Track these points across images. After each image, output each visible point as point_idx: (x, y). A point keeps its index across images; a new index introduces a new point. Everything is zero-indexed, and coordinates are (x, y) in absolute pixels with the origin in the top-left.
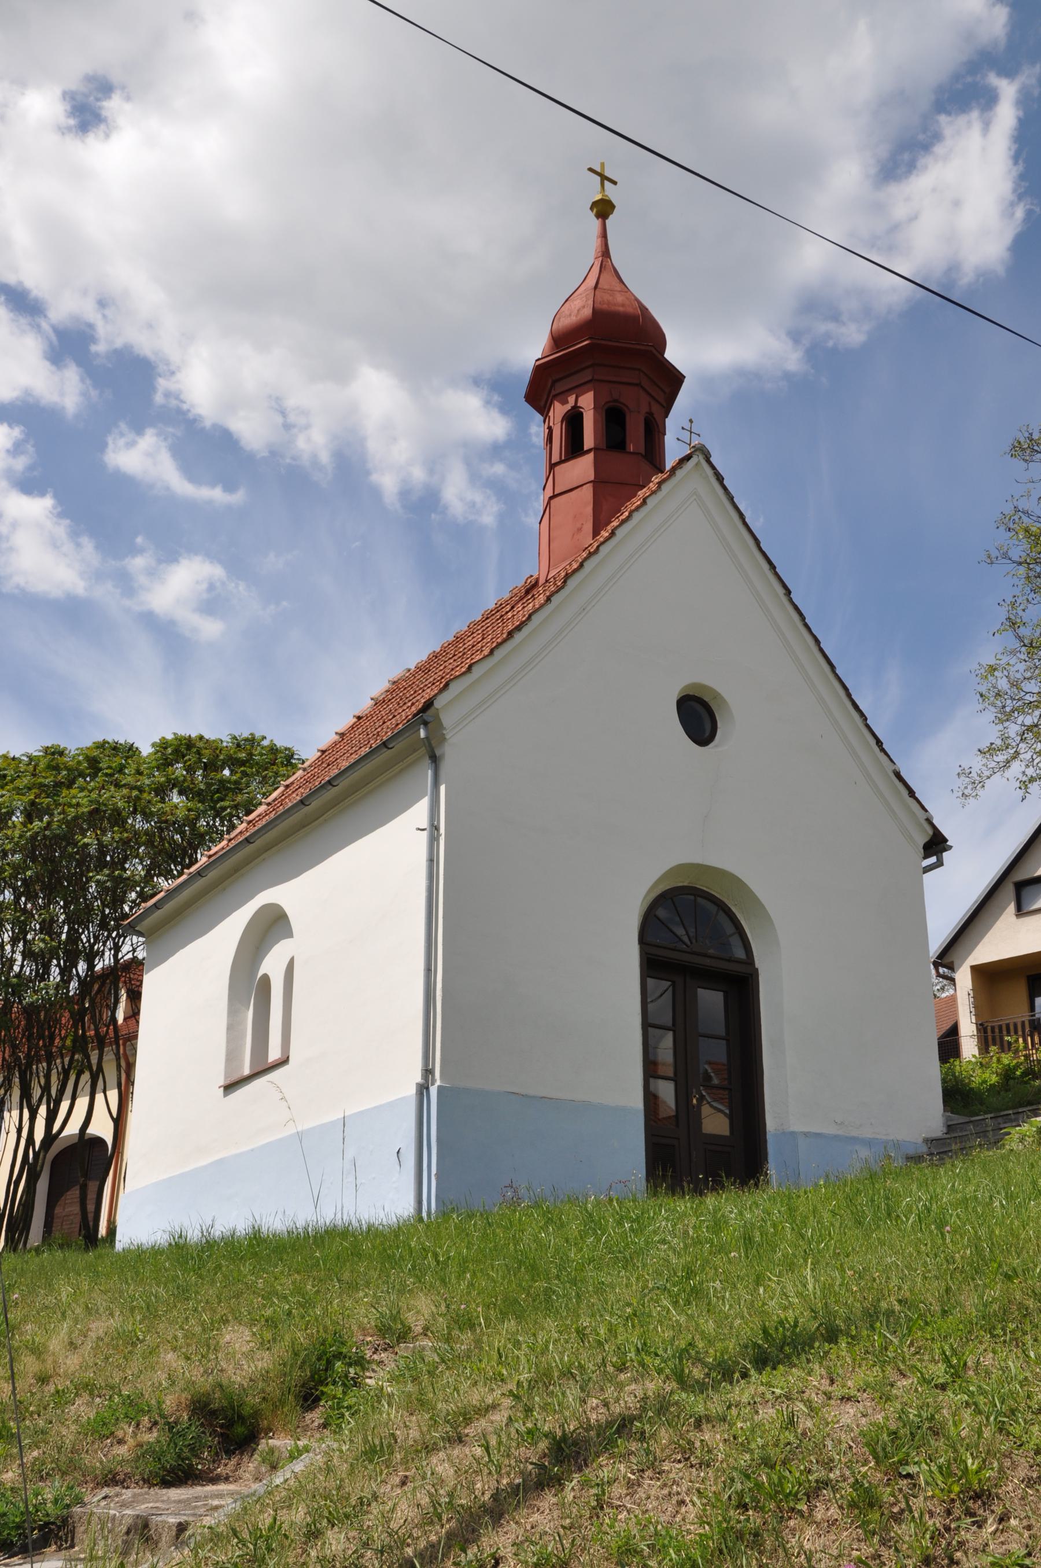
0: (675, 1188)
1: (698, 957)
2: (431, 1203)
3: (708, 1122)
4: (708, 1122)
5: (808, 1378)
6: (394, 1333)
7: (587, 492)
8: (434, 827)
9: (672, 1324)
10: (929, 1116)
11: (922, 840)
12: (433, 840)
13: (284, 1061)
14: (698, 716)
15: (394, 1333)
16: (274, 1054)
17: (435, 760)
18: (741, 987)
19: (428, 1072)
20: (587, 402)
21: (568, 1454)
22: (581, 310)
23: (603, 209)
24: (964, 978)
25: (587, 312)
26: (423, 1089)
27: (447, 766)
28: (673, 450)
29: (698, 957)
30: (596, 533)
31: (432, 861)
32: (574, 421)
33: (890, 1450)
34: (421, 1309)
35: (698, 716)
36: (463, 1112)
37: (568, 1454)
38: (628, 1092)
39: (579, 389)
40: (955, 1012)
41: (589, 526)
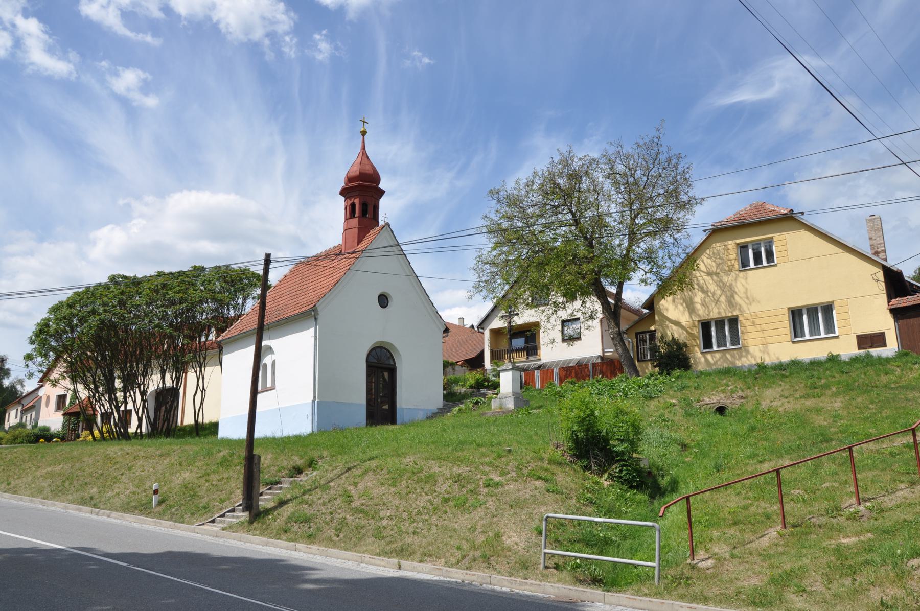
0: (371, 425)
1: (381, 368)
2: (316, 430)
3: (382, 404)
4: (382, 404)
5: (373, 462)
6: (321, 457)
7: (356, 230)
8: (316, 337)
9: (362, 456)
10: (437, 400)
11: (443, 329)
12: (315, 339)
13: (272, 388)
14: (383, 300)
15: (321, 457)
16: (269, 385)
17: (316, 319)
18: (392, 371)
19: (314, 397)
20: (357, 201)
21: (349, 469)
22: (356, 172)
23: (364, 133)
24: (487, 334)
25: (358, 173)
26: (313, 401)
27: (319, 321)
28: (381, 223)
29: (381, 368)
30: (359, 241)
31: (315, 345)
32: (353, 206)
33: (377, 467)
34: (325, 453)
35: (383, 300)
36: (323, 407)
37: (349, 469)
38: (363, 400)
39: (355, 197)
40: (483, 345)
41: (356, 241)
